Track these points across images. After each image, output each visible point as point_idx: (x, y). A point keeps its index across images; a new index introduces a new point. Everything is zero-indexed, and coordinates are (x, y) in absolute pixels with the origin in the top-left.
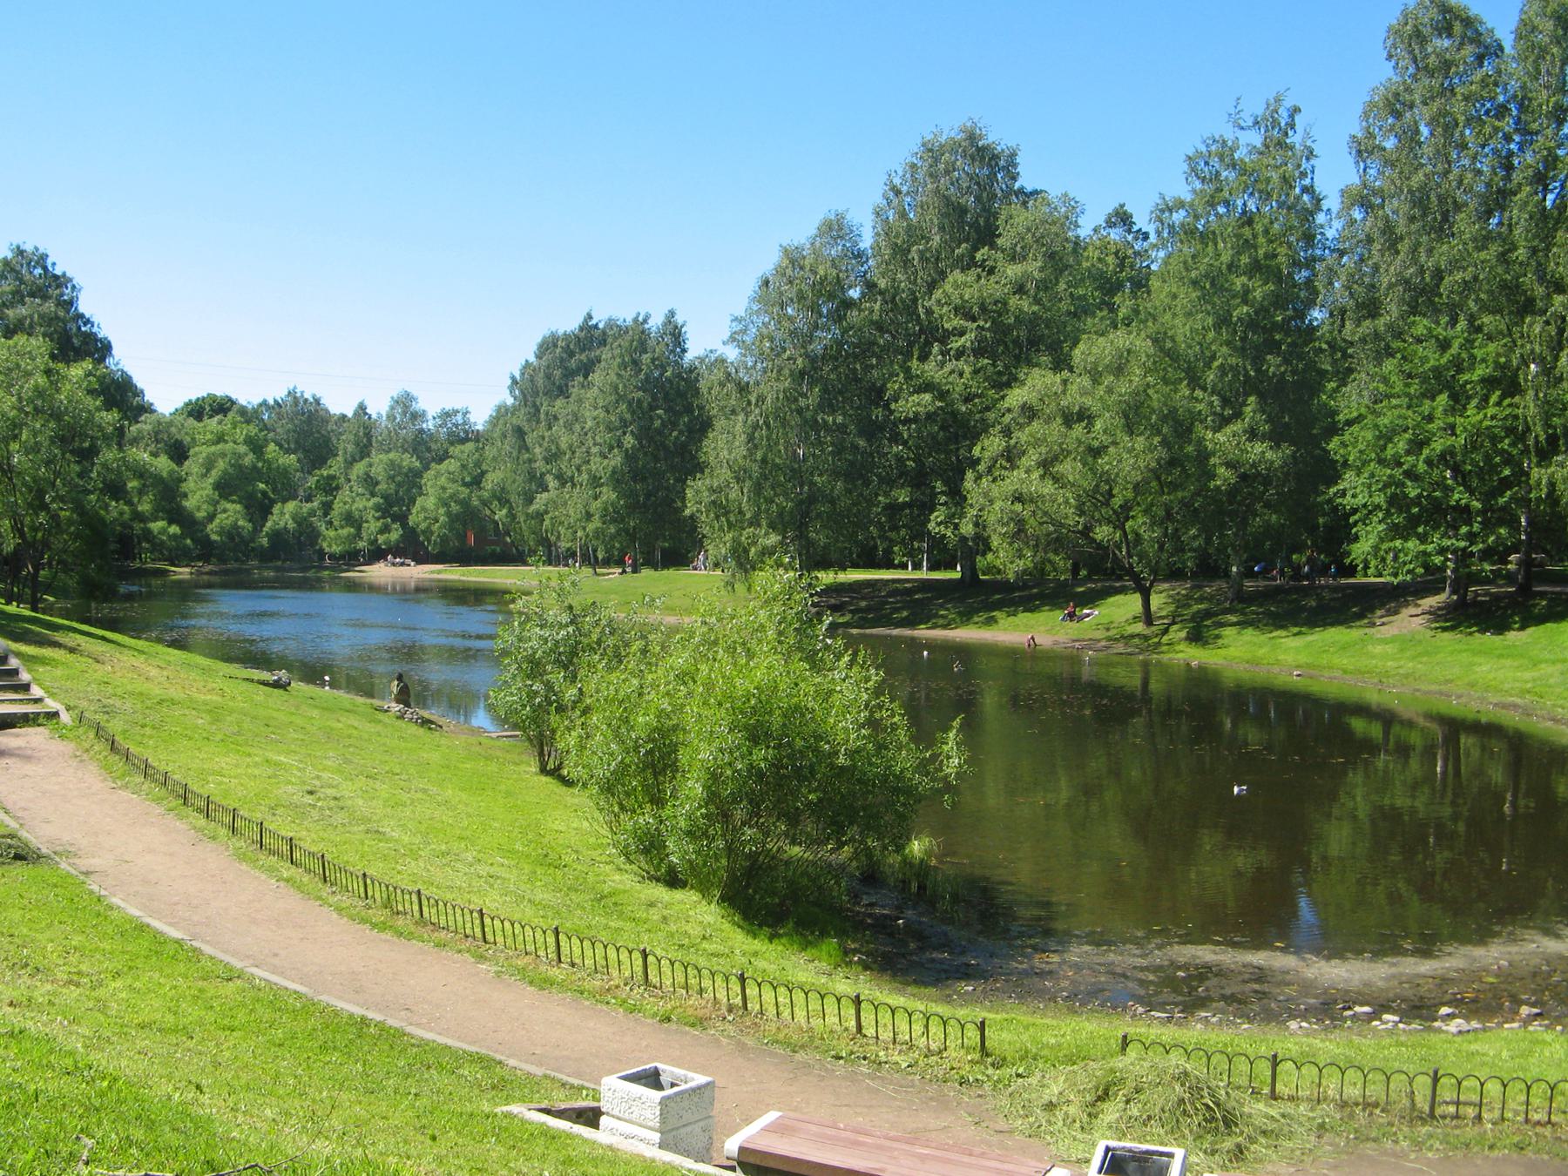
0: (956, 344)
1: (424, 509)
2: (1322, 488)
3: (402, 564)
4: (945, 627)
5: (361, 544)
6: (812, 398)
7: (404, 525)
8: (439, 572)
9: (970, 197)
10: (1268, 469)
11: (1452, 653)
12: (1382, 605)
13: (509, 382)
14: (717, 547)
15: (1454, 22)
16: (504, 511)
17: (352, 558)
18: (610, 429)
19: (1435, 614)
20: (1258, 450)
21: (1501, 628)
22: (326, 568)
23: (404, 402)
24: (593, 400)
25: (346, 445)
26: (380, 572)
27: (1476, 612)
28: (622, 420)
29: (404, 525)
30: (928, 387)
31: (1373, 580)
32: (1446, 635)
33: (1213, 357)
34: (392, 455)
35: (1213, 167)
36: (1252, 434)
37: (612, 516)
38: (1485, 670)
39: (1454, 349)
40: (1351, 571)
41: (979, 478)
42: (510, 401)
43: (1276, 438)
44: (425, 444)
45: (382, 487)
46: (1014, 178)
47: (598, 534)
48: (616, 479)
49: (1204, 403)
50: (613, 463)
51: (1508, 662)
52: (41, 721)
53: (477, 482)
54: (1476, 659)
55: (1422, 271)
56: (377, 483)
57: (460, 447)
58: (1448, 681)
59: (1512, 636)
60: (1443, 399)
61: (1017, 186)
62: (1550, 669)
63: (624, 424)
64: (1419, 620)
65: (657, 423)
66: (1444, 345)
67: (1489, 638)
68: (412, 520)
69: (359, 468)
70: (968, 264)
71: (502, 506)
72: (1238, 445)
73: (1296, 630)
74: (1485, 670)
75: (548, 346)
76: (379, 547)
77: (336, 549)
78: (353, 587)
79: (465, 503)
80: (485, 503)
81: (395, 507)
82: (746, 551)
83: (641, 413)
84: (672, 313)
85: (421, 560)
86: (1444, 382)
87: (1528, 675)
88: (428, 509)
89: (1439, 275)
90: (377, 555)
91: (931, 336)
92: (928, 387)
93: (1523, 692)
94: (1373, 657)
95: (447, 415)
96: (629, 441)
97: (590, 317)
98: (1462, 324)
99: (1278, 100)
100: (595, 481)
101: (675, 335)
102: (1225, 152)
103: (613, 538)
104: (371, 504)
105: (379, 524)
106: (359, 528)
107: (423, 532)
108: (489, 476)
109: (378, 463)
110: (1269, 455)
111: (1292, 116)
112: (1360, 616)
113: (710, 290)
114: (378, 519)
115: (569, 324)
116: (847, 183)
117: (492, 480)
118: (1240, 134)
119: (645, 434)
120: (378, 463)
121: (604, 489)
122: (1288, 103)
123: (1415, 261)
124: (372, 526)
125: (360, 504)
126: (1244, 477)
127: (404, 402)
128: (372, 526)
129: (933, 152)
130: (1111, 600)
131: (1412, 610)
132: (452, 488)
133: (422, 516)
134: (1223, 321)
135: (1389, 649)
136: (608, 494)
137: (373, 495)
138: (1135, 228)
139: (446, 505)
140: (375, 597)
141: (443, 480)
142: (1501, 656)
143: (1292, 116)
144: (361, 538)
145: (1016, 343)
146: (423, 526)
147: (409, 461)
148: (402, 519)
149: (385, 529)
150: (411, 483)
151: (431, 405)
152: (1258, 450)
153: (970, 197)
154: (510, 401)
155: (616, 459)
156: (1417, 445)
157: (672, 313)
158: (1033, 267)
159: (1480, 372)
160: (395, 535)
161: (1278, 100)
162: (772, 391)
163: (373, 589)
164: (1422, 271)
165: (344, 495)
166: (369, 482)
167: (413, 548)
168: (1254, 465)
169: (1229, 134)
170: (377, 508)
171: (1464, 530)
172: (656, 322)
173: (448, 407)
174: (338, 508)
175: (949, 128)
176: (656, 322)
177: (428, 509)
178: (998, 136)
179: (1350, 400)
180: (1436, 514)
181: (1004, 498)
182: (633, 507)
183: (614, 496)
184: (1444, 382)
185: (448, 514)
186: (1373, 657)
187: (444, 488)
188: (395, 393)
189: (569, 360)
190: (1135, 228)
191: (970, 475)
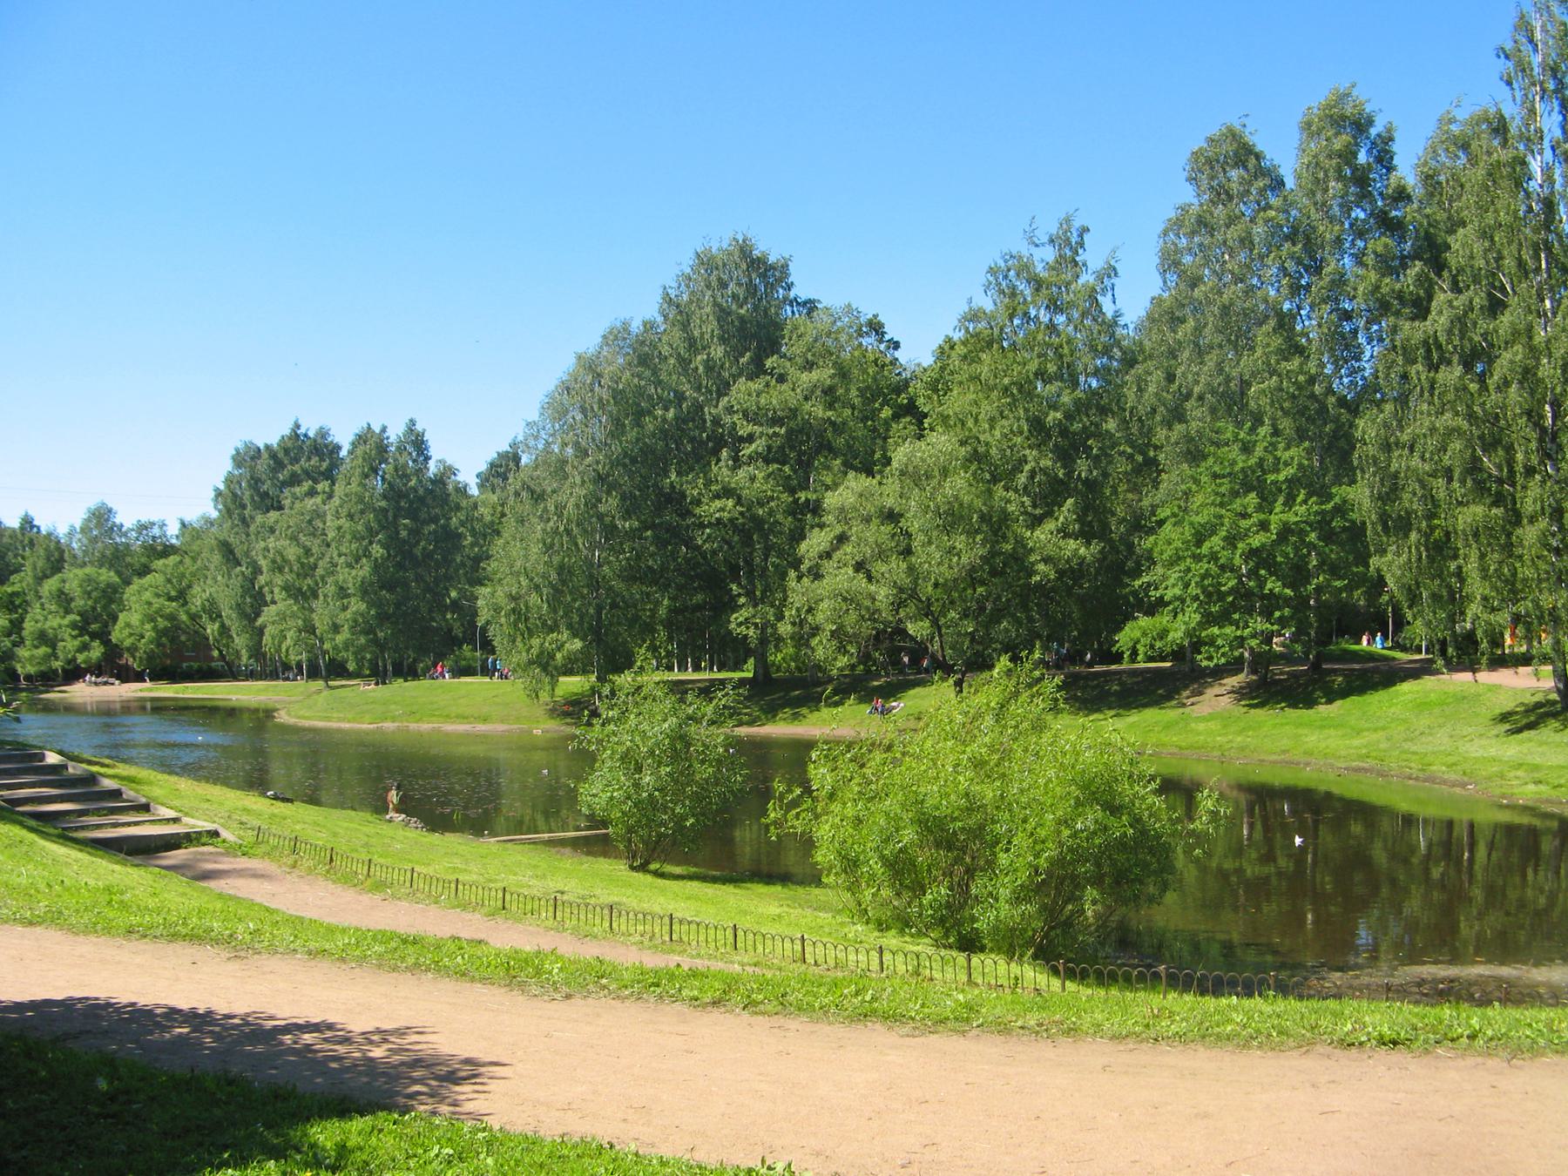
0: (748, 450)
1: (128, 625)
2: (1127, 581)
3: (106, 683)
4: (751, 723)
5: (57, 664)
6: (610, 504)
7: (106, 642)
8: (151, 690)
9: (747, 309)
10: (1080, 564)
11: (1275, 726)
12: (1186, 687)
13: (213, 494)
14: (511, 655)
15: (1244, 154)
16: (217, 625)
17: (48, 679)
18: (356, 537)
19: (1241, 694)
20: (1073, 547)
21: (1310, 703)
22: (23, 690)
23: (101, 517)
24: (335, 510)
25: (33, 562)
26: (82, 692)
27: (1271, 688)
28: (369, 529)
29: (106, 642)
30: (727, 492)
31: (1142, 665)
32: (1258, 711)
33: (1024, 460)
34: (88, 570)
35: (1012, 280)
36: (1064, 533)
37: (364, 627)
38: (1312, 739)
39: (1259, 451)
40: (1118, 658)
41: (799, 578)
42: (215, 514)
43: (1086, 535)
44: (124, 556)
45: (79, 603)
46: (789, 287)
47: (347, 645)
48: (365, 591)
49: (1014, 503)
50: (361, 573)
51: (1332, 732)
52: (204, 840)
53: (182, 596)
54: (1300, 731)
55: (1228, 380)
56: (72, 599)
57: (162, 562)
58: (1284, 752)
59: (1323, 710)
60: (1252, 499)
61: (792, 295)
62: (1375, 736)
63: (372, 533)
64: (1226, 699)
65: (404, 534)
66: (1247, 449)
67: (1292, 714)
68: (117, 634)
69: (51, 585)
70: (757, 370)
71: (212, 620)
72: (1052, 542)
73: (1112, 712)
74: (1312, 739)
75: (247, 457)
76: (78, 667)
77: (31, 669)
78: (50, 708)
79: (172, 617)
80: (194, 617)
81: (96, 620)
82: (552, 656)
83: (386, 521)
84: (413, 422)
85: (126, 675)
86: (1250, 482)
87: (1356, 742)
88: (133, 624)
89: (1245, 385)
90: (73, 674)
91: (722, 441)
92: (727, 492)
93: (1361, 757)
94: (1199, 734)
95: (143, 527)
96: (377, 551)
97: (298, 426)
98: (1263, 431)
99: (1068, 221)
100: (342, 592)
101: (417, 443)
102: (1024, 269)
103: (363, 649)
104: (66, 621)
105: (76, 643)
106: (54, 647)
107: (128, 649)
108: (196, 589)
109: (73, 579)
110: (1082, 551)
111: (1081, 236)
112: (1169, 697)
113: (482, 392)
114: (75, 637)
115: (270, 435)
116: (629, 287)
117: (198, 597)
118: (1034, 250)
119: (393, 543)
120: (73, 579)
121: (353, 600)
122: (1077, 224)
123: (1221, 371)
124: (69, 645)
125: (54, 622)
126: (1061, 574)
127: (101, 517)
128: (69, 645)
129: (706, 262)
130: (912, 692)
131: (1217, 690)
132: (158, 603)
133: (126, 632)
134: (1037, 424)
135: (1212, 725)
136: (357, 605)
137: (68, 611)
138: (887, 337)
139: (153, 620)
140: (72, 719)
141: (147, 595)
142: (1322, 727)
143: (1081, 236)
144: (57, 659)
145: (803, 449)
146: (127, 643)
147: (107, 576)
148: (103, 636)
149: (85, 647)
150: (108, 601)
151: (44, 523)
152: (1073, 547)
153: (747, 309)
154: (215, 514)
155: (364, 570)
156: (1231, 541)
157: (413, 422)
158: (823, 375)
159: (1289, 472)
160: (96, 652)
161: (1068, 221)
162: (573, 494)
163: (70, 709)
164: (1228, 380)
165: (36, 611)
166: (63, 600)
167: (113, 667)
168: (1068, 561)
169: (1024, 250)
170: (74, 625)
171: (1277, 614)
172: (395, 433)
173: (144, 520)
174: (29, 626)
175: (719, 240)
176: (395, 433)
177: (133, 624)
178: (770, 247)
179: (1160, 497)
180: (1246, 600)
181: (827, 593)
182: (383, 618)
183: (364, 606)
184: (1250, 482)
185: (155, 628)
186: (1199, 734)
187: (150, 604)
188: (93, 503)
189: (279, 474)
190: (887, 337)
191: (792, 574)
